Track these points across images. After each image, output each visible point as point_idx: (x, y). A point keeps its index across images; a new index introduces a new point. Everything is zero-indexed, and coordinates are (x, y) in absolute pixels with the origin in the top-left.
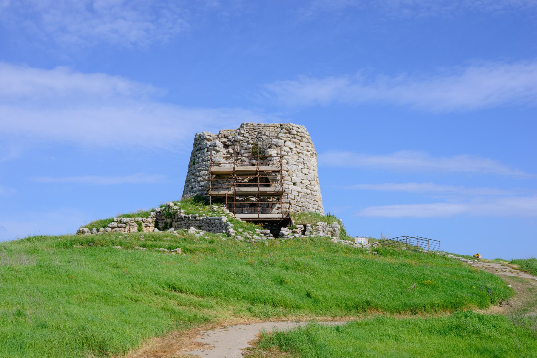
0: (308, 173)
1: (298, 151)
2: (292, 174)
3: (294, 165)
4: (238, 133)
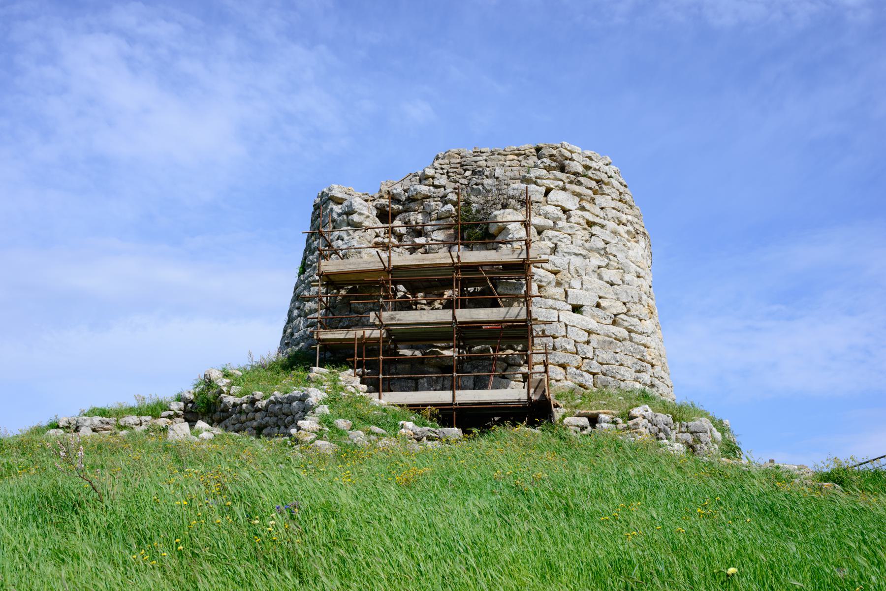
0: (620, 282)
1: (587, 217)
2: (568, 280)
3: (576, 254)
4: (418, 178)
